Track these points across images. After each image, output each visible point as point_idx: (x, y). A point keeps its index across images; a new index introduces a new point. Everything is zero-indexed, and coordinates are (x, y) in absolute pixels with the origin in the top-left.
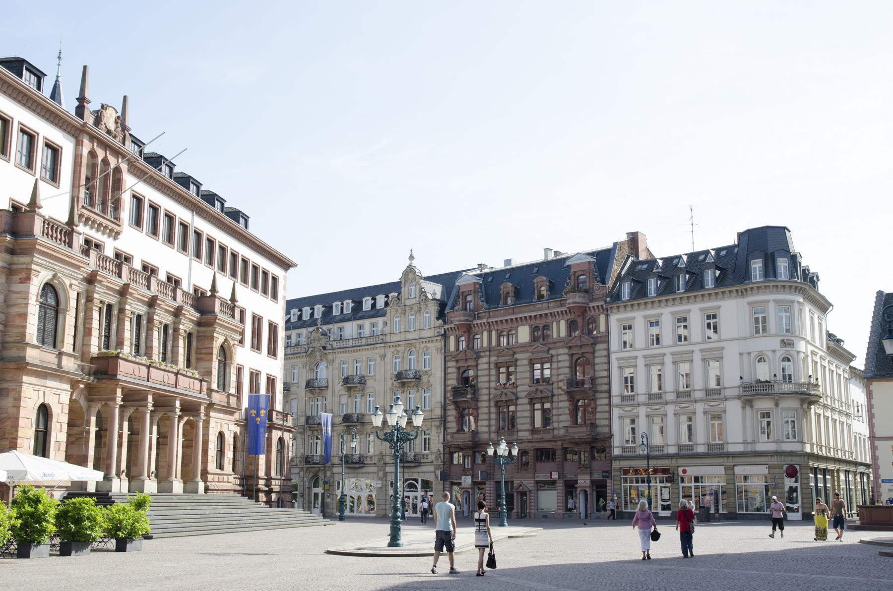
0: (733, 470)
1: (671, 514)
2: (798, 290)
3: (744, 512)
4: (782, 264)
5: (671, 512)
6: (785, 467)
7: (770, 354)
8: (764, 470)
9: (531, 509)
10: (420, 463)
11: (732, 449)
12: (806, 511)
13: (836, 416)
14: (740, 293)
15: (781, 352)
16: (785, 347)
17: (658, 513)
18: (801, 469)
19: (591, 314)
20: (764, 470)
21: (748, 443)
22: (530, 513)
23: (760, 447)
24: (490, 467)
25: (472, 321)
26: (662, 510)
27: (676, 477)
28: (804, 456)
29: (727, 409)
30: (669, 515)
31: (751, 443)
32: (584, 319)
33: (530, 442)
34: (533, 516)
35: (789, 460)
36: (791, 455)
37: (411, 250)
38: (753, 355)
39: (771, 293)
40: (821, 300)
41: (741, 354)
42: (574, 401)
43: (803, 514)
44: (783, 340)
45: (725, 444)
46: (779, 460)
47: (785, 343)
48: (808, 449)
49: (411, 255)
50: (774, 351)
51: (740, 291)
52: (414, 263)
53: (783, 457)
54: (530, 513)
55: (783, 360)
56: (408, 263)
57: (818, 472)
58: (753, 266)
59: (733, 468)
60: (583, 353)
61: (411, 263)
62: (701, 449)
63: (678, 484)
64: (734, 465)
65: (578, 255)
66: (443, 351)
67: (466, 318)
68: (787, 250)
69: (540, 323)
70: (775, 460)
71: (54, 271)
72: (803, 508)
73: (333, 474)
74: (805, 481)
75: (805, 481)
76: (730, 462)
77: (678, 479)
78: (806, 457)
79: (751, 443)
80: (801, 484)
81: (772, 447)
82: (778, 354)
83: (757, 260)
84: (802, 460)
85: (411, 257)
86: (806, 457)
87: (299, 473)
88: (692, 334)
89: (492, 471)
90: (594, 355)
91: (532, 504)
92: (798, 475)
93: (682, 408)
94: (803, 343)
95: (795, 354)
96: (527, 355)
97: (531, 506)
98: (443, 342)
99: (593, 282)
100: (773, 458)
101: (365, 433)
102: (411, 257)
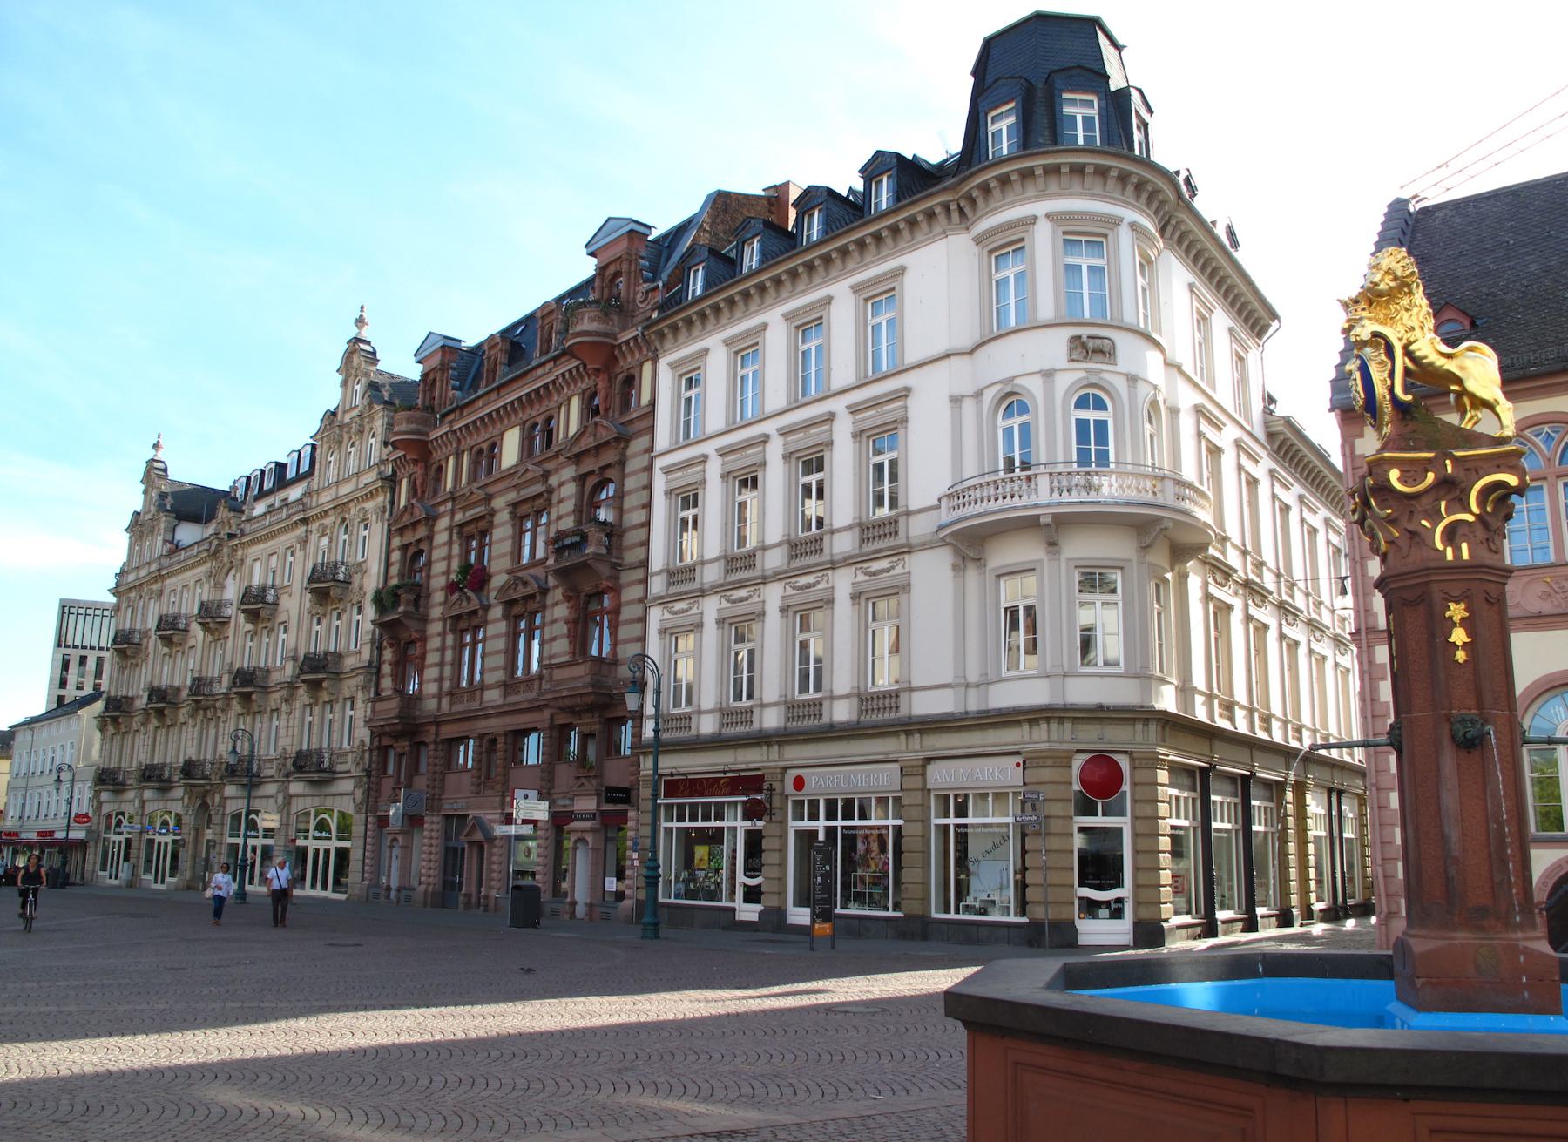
0: (923, 775)
1: (761, 914)
2: (1144, 196)
3: (891, 913)
4: (1080, 110)
5: (759, 907)
6: (1078, 762)
7: (1035, 386)
8: (1006, 772)
9: (491, 888)
10: (335, 772)
11: (924, 705)
12: (1146, 914)
13: (1297, 632)
14: (955, 216)
15: (1070, 377)
16: (1086, 359)
17: (734, 910)
18: (1134, 768)
19: (626, 366)
20: (1006, 772)
21: (968, 686)
22: (486, 897)
23: (1005, 697)
24: (435, 780)
25: (427, 434)
26: (746, 901)
27: (776, 801)
28: (1146, 721)
29: (914, 581)
30: (755, 917)
31: (977, 686)
32: (610, 380)
33: (500, 713)
34: (492, 904)
35: (1092, 737)
36: (1100, 720)
37: (362, 307)
38: (989, 396)
39: (1043, 195)
40: (1317, 462)
41: (956, 400)
42: (578, 597)
43: (1138, 925)
44: (1079, 337)
45: (905, 690)
46: (1054, 736)
47: (1084, 345)
48: (1167, 700)
49: (361, 316)
50: (1048, 374)
51: (953, 207)
52: (366, 333)
53: (1068, 725)
54: (486, 897)
55: (1082, 403)
56: (353, 332)
57: (1213, 785)
58: (992, 128)
59: (924, 767)
60: (603, 468)
61: (360, 333)
62: (842, 712)
63: (783, 822)
64: (929, 760)
65: (611, 223)
66: (387, 514)
67: (413, 426)
68: (1096, 67)
69: (536, 412)
70: (1040, 737)
71: (1017, 753)
72: (1137, 904)
73: (224, 799)
74: (1147, 810)
75: (1147, 810)
76: (916, 747)
77: (784, 809)
78: (1153, 727)
79: (977, 686)
80: (1135, 818)
81: (1035, 694)
82: (1063, 382)
83: (1003, 109)
84: (1139, 737)
85: (360, 322)
86: (1153, 727)
87: (182, 799)
88: (832, 366)
89: (436, 791)
90: (623, 470)
91: (494, 875)
92: (1126, 787)
93: (801, 588)
94: (1153, 361)
95: (1120, 384)
96: (512, 496)
97: (492, 879)
98: (388, 495)
99: (636, 284)
100: (1035, 730)
101: (269, 709)
102: (360, 322)
